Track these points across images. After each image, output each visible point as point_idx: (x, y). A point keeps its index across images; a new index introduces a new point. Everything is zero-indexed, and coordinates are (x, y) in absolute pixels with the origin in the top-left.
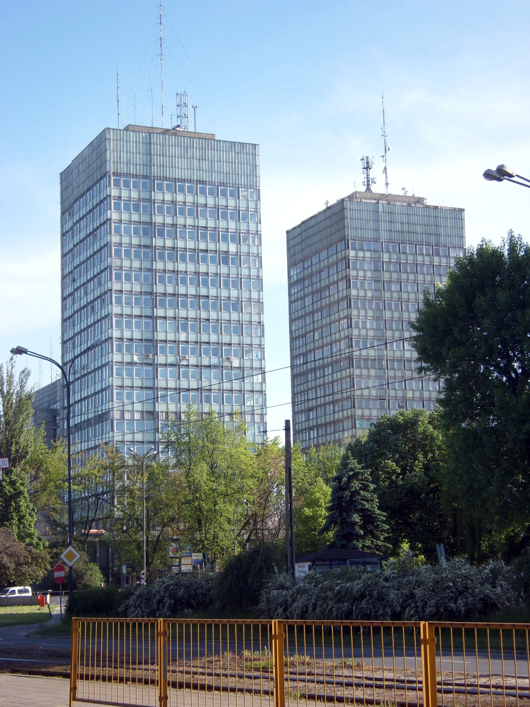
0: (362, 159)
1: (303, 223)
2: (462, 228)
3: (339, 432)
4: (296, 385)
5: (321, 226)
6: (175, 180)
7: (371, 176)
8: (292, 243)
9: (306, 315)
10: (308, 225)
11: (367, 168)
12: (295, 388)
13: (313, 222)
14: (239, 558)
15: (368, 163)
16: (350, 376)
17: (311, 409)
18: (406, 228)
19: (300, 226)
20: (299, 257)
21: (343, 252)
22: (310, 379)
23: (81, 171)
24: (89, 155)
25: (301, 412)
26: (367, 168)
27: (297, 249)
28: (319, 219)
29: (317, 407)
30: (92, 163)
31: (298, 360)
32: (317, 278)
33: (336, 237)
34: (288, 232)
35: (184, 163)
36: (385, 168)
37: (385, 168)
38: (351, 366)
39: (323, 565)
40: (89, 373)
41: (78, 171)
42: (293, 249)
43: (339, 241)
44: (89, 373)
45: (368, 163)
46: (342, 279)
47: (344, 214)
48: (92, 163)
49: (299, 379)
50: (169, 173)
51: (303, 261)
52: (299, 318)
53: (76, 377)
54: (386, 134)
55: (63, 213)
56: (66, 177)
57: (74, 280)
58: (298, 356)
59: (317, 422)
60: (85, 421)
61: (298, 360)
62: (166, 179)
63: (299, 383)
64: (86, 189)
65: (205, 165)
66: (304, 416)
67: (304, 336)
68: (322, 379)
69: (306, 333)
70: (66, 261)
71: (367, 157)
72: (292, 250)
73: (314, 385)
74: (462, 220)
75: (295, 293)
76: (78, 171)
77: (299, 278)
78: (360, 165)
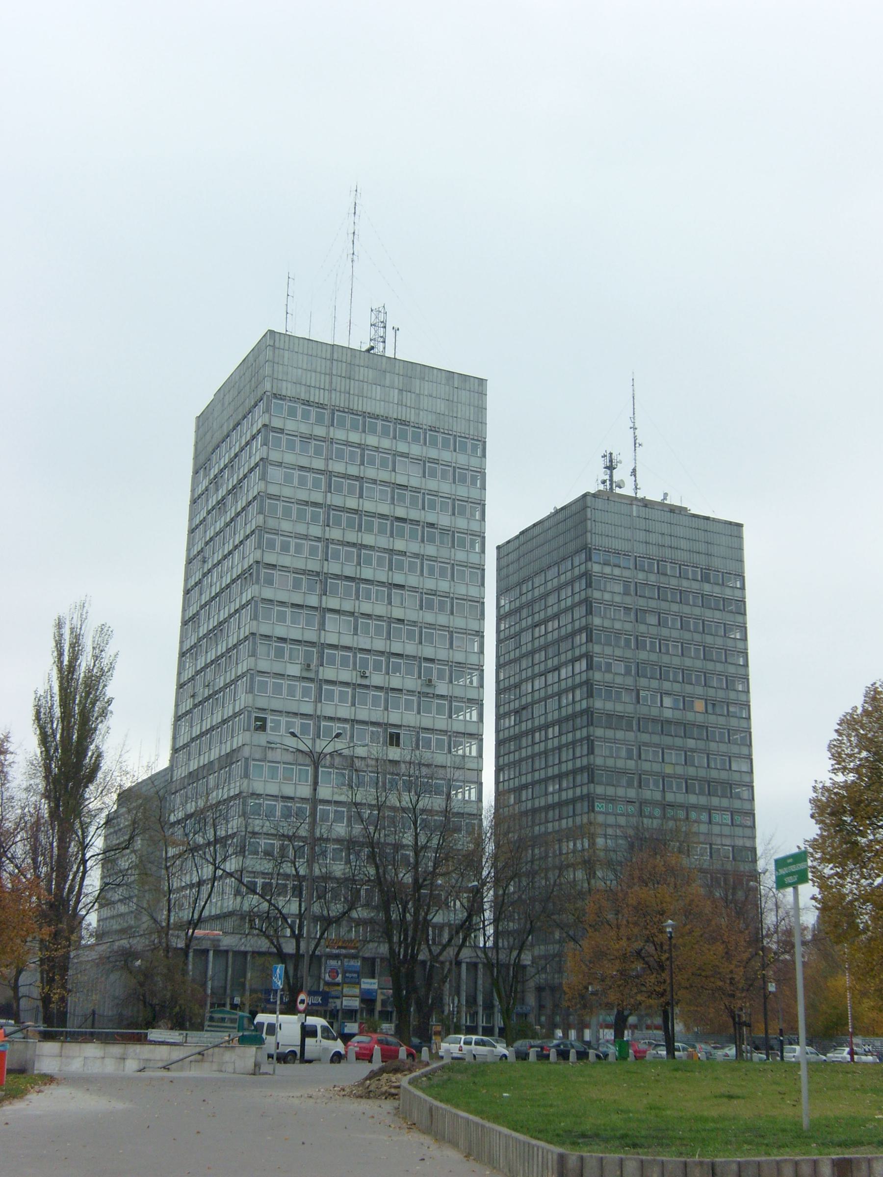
0: (605, 456)
1: (522, 533)
2: (741, 549)
3: (567, 818)
4: (502, 753)
5: (551, 533)
6: (364, 414)
7: (615, 479)
8: (504, 562)
9: (523, 656)
10: (529, 535)
11: (610, 468)
12: (501, 759)
13: (536, 531)
14: (394, 993)
15: (611, 461)
16: (588, 738)
17: (525, 787)
18: (667, 541)
19: (517, 537)
20: (514, 579)
21: (583, 566)
22: (524, 745)
23: (226, 404)
24: (241, 377)
25: (509, 791)
26: (610, 468)
27: (511, 569)
28: (547, 525)
29: (533, 784)
30: (245, 386)
31: (507, 720)
32: (540, 606)
33: (572, 547)
34: (498, 548)
35: (378, 392)
36: (634, 470)
37: (634, 470)
38: (591, 723)
39: (226, 978)
40: (216, 693)
41: (223, 405)
42: (505, 570)
43: (577, 552)
44: (216, 693)
45: (611, 461)
46: (580, 603)
47: (586, 515)
48: (245, 386)
49: (507, 745)
50: (358, 405)
51: (520, 584)
52: (511, 662)
53: (196, 702)
54: (636, 426)
55: (196, 472)
56: (203, 420)
57: (204, 561)
58: (507, 715)
59: (533, 804)
60: (204, 765)
61: (507, 720)
62: (352, 412)
63: (507, 751)
64: (231, 427)
65: (409, 399)
66: (512, 796)
67: (517, 686)
68: (542, 744)
69: (521, 682)
70: (193, 538)
71: (611, 454)
72: (504, 571)
73: (529, 753)
74: (740, 537)
75: (505, 629)
76: (223, 405)
77: (513, 607)
78: (601, 463)
